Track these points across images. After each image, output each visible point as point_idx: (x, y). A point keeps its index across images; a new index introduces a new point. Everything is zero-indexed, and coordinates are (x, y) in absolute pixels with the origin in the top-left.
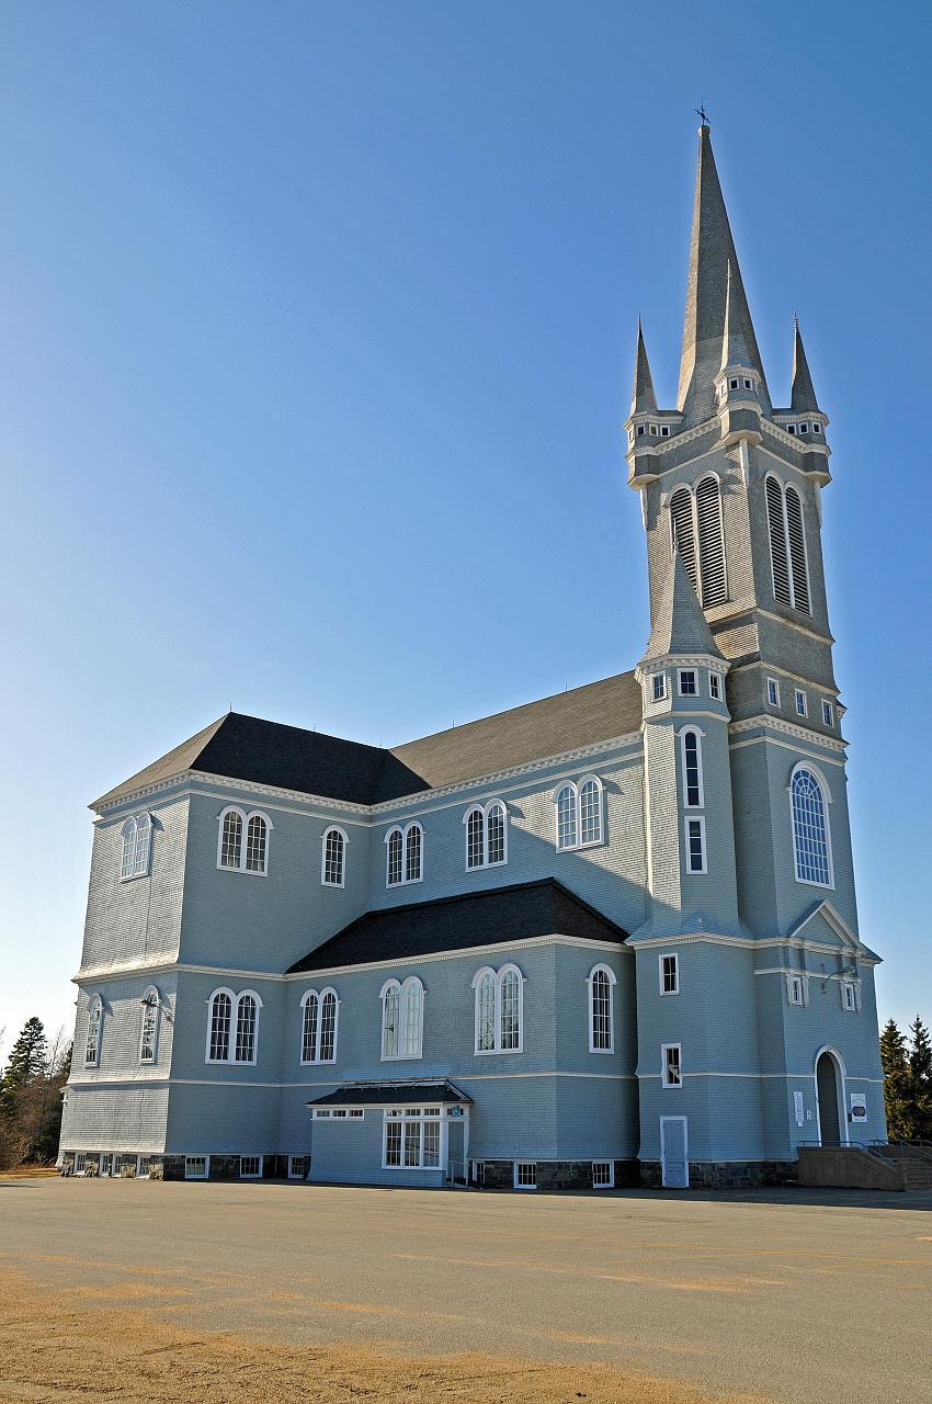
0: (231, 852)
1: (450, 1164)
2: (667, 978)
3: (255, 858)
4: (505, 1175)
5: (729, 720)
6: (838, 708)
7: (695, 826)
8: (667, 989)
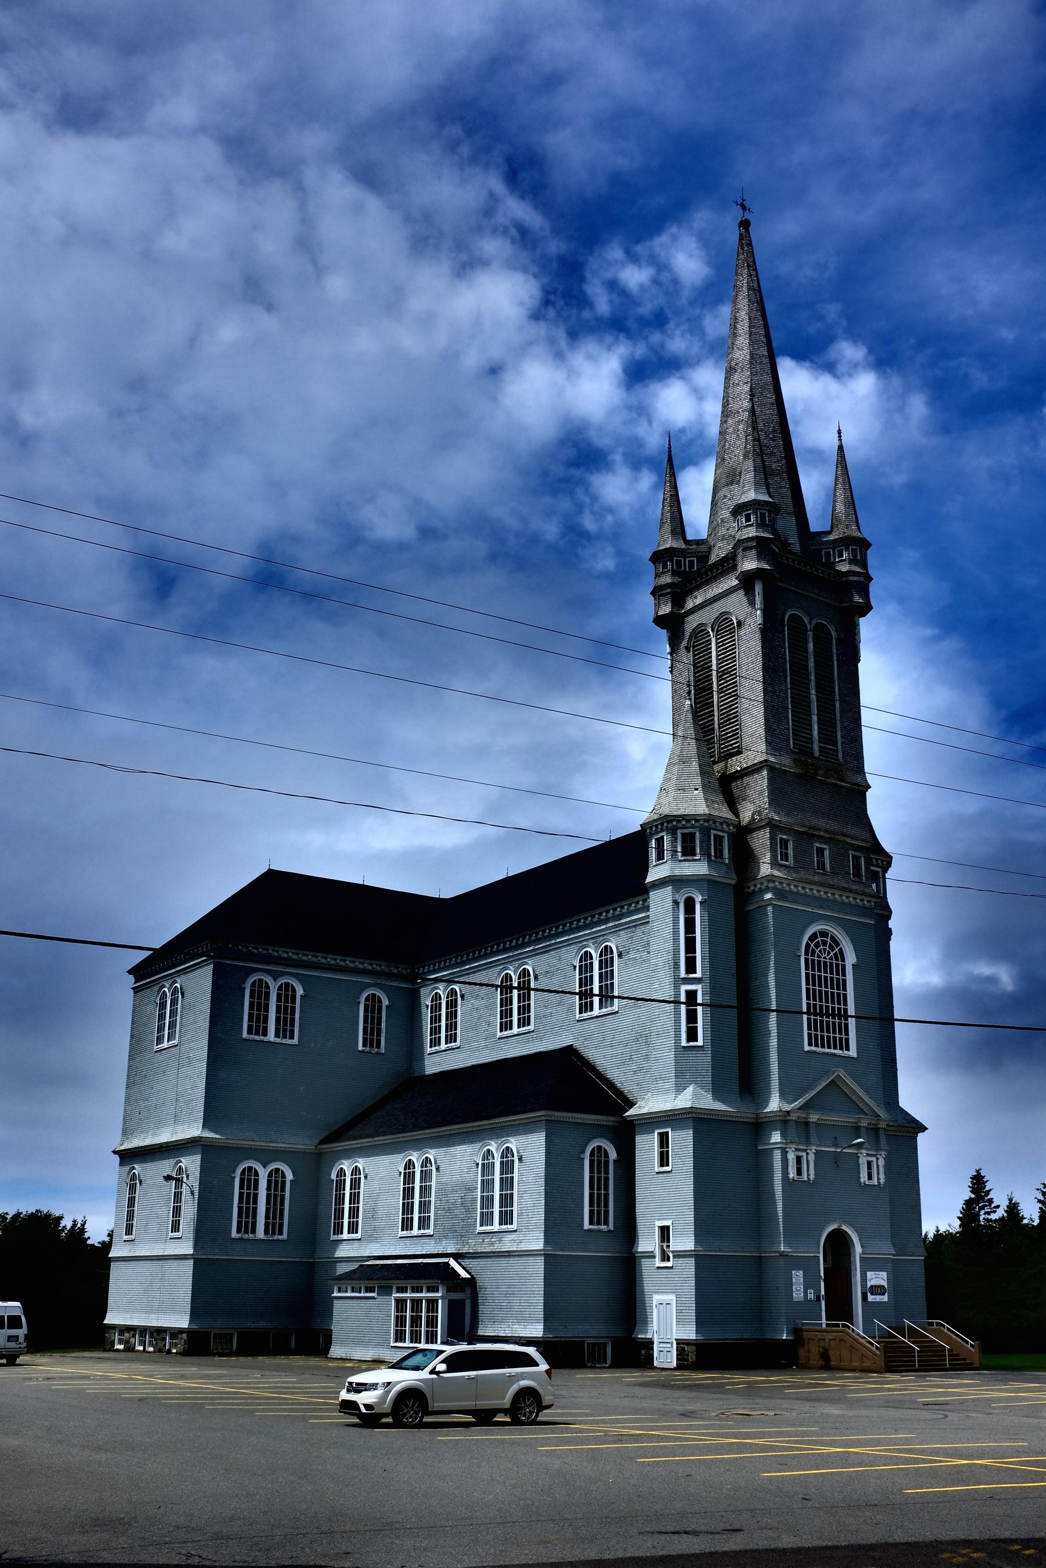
2: (662, 1154)
3: (284, 1027)
8: (662, 1165)
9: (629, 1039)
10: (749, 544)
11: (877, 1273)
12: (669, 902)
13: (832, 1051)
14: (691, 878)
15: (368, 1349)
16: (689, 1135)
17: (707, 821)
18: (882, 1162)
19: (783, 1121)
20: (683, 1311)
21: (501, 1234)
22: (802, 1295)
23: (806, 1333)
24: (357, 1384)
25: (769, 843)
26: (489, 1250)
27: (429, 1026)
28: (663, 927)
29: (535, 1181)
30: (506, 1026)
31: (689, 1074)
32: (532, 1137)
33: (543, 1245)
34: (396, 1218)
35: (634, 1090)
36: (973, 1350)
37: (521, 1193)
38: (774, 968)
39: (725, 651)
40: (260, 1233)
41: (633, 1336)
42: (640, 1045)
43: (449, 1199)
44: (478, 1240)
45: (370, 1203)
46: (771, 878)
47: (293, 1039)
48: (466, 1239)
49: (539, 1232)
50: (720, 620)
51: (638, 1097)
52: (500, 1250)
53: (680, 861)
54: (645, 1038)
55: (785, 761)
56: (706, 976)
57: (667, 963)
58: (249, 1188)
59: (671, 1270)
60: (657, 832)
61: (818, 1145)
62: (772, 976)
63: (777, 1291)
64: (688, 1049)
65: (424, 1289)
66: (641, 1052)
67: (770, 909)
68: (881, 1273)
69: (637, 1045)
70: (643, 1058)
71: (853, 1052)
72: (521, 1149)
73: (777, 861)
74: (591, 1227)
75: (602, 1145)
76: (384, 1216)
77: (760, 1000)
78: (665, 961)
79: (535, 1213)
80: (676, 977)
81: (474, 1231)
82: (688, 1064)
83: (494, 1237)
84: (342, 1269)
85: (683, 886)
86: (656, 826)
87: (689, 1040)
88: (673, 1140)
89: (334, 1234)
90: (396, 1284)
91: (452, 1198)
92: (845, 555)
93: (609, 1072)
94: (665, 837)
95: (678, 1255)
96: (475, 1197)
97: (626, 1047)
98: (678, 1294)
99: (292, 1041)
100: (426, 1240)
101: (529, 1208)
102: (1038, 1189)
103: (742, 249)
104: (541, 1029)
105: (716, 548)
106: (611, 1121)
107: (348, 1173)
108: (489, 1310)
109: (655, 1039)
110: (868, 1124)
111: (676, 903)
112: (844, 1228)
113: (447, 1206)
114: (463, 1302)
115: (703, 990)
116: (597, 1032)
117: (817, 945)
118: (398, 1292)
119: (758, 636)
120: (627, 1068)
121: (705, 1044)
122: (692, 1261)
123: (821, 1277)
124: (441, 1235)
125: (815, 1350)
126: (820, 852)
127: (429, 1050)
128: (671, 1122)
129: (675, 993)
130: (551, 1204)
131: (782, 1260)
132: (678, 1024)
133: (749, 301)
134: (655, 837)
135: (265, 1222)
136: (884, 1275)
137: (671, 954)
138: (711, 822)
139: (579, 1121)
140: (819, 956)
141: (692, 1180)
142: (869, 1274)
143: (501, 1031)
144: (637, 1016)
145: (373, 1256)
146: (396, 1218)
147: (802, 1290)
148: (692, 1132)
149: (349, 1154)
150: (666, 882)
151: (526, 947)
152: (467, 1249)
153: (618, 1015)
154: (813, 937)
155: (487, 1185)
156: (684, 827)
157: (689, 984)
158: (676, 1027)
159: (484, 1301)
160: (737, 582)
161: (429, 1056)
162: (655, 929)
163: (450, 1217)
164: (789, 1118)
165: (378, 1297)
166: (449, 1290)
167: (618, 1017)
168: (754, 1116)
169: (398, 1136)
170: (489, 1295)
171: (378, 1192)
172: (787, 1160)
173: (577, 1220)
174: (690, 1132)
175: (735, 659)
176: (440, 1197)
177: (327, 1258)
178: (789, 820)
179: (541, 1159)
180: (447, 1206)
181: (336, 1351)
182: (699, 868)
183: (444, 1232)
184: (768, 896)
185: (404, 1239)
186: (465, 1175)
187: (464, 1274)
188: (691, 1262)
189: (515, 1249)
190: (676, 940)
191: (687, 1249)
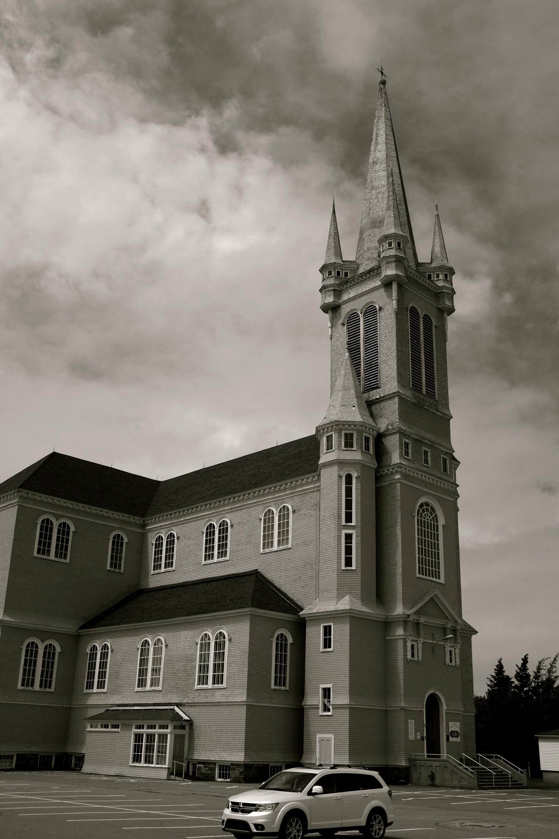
0: (44, 548)
1: (173, 763)
2: (325, 640)
3: (61, 551)
4: (210, 772)
5: (375, 467)
6: (453, 462)
7: (349, 537)
8: (325, 647)
10: (390, 260)
11: (455, 723)
12: (335, 476)
13: (431, 578)
14: (350, 461)
15: (111, 767)
16: (347, 628)
17: (361, 426)
18: (458, 651)
19: (405, 621)
20: (339, 745)
21: (214, 690)
22: (414, 736)
23: (418, 761)
24: (244, 804)
25: (398, 444)
26: (204, 701)
27: (153, 557)
28: (331, 492)
29: (241, 655)
30: (209, 557)
33: (246, 698)
34: (134, 679)
35: (302, 599)
36: (522, 775)
37: (229, 663)
38: (400, 522)
39: (369, 325)
40: (37, 687)
41: (301, 762)
42: (307, 569)
43: (175, 666)
44: (195, 695)
45: (115, 668)
46: (399, 465)
47: (66, 559)
48: (187, 693)
49: (243, 689)
50: (367, 307)
51: (305, 603)
52: (213, 701)
53: (343, 450)
54: (311, 565)
55: (408, 394)
56: (358, 525)
57: (333, 515)
58: (31, 656)
59: (331, 718)
60: (327, 432)
61: (425, 638)
62: (399, 527)
63: (398, 733)
64: (346, 572)
65: (157, 727)
66: (307, 574)
67: (398, 485)
68: (457, 723)
69: (305, 570)
70: (309, 578)
71: (442, 580)
72: (231, 633)
73: (403, 455)
74: (276, 687)
75: (284, 633)
76: (125, 677)
77: (389, 543)
78: (331, 514)
80: (339, 524)
81: (193, 688)
83: (208, 692)
84: (92, 712)
85: (344, 467)
86: (328, 428)
87: (346, 566)
88: (334, 630)
89: (87, 689)
90: (158, 723)
91: (176, 666)
92: (441, 277)
93: (283, 587)
94: (333, 435)
95: (336, 707)
96: (194, 665)
97: (297, 571)
98: (335, 733)
99: (66, 560)
100: (156, 694)
101: (236, 673)
102: (488, 678)
103: (381, 96)
104: (235, 559)
105: (364, 265)
106: (290, 618)
107: (99, 649)
108: (202, 742)
111: (340, 477)
112: (437, 693)
113: (172, 671)
114: (183, 736)
117: (423, 511)
118: (136, 728)
119: (393, 316)
120: (297, 585)
121: (357, 568)
122: (347, 711)
123: (424, 724)
124: (167, 690)
125: (425, 774)
126: (426, 453)
127: (152, 572)
130: (251, 671)
131: (403, 712)
132: (339, 555)
133: (386, 125)
134: (326, 435)
135: (41, 679)
136: (458, 724)
137: (335, 509)
138: (364, 428)
139: (271, 616)
140: (424, 518)
141: (349, 657)
142: (450, 723)
143: (205, 560)
144: (305, 551)
145: (115, 704)
146: (134, 679)
147: (414, 733)
148: (349, 626)
149: (99, 636)
150: (333, 464)
151: (226, 507)
152: (187, 700)
153: (291, 550)
154: (421, 506)
155: (204, 658)
157: (347, 529)
158: (338, 557)
159: (199, 736)
160: (380, 283)
161: (153, 576)
162: (324, 494)
163: (175, 678)
164: (409, 619)
165: (121, 732)
166: (175, 727)
169: (138, 624)
170: (202, 732)
171: (121, 661)
172: (406, 647)
173: (267, 682)
174: (347, 626)
175: (377, 330)
176: (168, 665)
177: (80, 705)
178: (410, 430)
180: (172, 671)
181: (87, 768)
182: (355, 455)
183: (170, 689)
184: (398, 476)
185: (139, 693)
186: (187, 651)
187: (186, 717)
188: (346, 712)
189: (224, 701)
190: (339, 501)
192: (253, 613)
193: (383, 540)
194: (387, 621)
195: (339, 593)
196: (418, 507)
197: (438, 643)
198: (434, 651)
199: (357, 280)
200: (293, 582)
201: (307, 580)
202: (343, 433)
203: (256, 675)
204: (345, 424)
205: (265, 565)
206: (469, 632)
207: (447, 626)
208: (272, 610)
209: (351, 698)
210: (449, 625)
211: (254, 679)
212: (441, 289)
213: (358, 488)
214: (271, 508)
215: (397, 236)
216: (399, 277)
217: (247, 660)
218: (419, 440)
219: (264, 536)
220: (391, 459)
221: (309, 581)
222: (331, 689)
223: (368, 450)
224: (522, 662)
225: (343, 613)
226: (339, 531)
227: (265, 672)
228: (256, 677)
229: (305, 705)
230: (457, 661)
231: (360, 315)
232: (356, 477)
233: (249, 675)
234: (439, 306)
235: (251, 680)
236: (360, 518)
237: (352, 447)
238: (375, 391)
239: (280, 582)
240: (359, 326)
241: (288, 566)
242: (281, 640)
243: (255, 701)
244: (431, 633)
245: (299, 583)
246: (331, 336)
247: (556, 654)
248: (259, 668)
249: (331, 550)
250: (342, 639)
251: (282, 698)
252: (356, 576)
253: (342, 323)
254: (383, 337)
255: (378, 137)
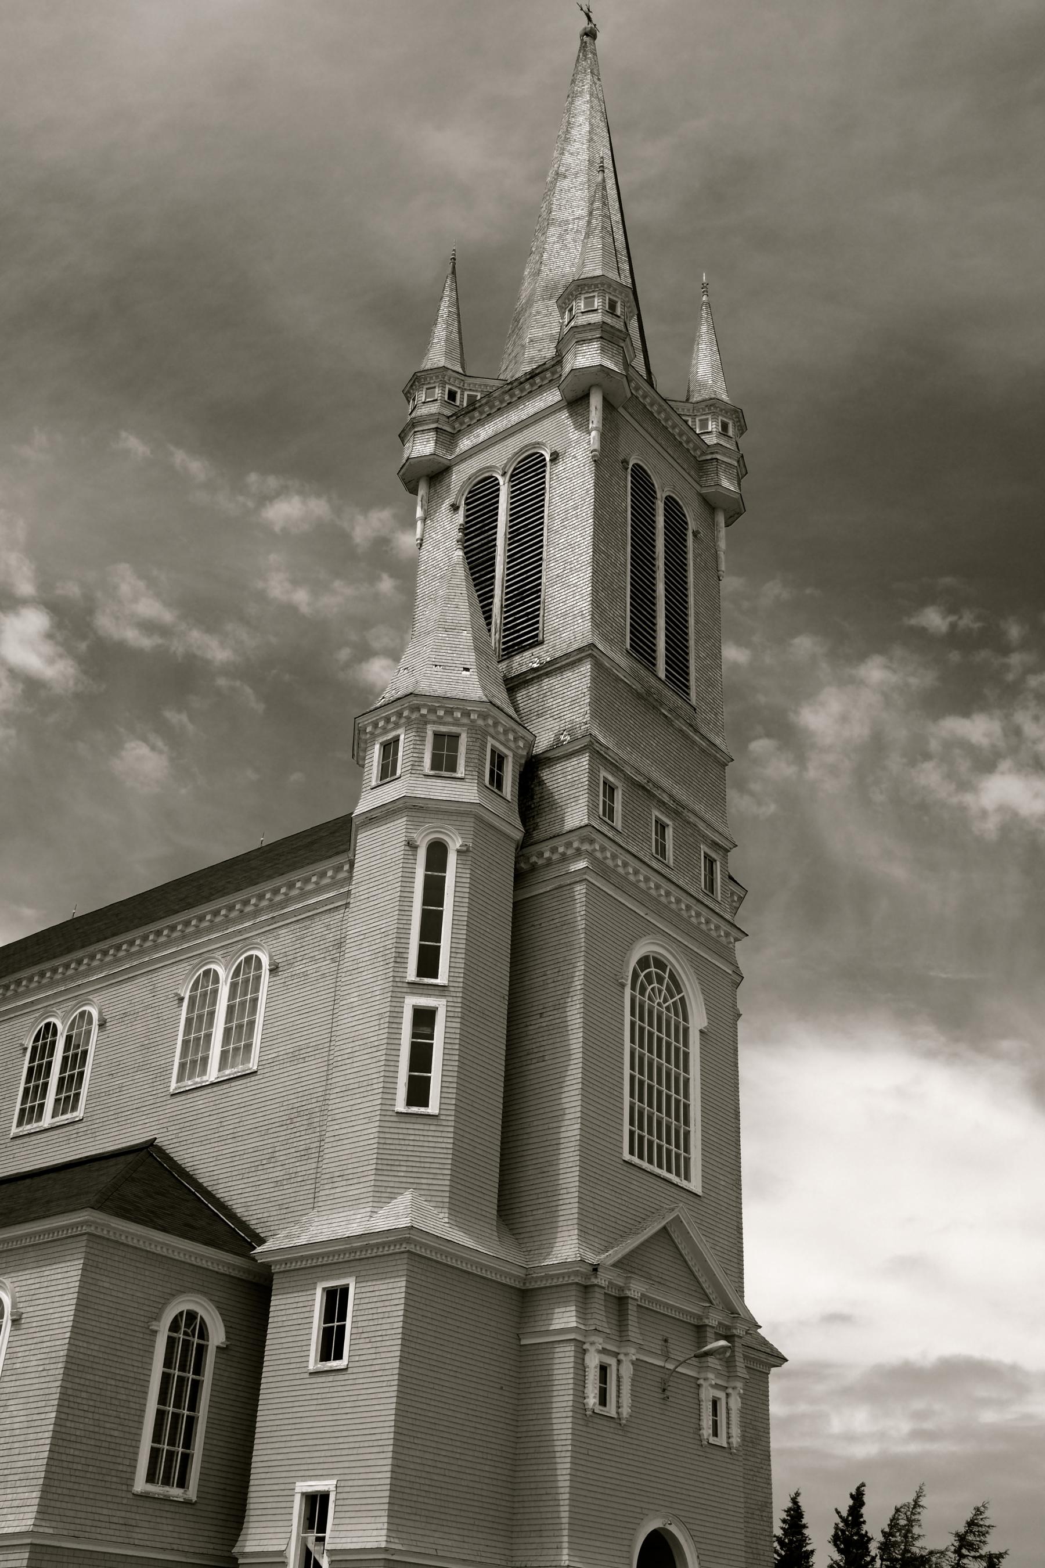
2: (327, 1333)
7: (424, 1018)
8: (325, 1357)
9: (273, 1121)
14: (444, 806)
16: (397, 1290)
17: (484, 716)
18: (735, 1403)
29: (41, 1368)
30: (30, 1113)
31: (404, 1169)
32: (53, 1272)
55: (620, 659)
56: (456, 985)
60: (385, 731)
64: (407, 1119)
67: (580, 890)
70: (298, 1154)
71: (695, 1184)
72: (23, 1299)
74: (152, 1488)
79: (29, 1443)
80: (397, 979)
82: (404, 1148)
86: (387, 720)
87: (410, 1102)
88: (357, 1302)
92: (711, 426)
94: (402, 737)
101: (17, 1432)
109: (338, 1100)
110: (720, 1323)
111: (411, 846)
112: (673, 1529)
115: (449, 1009)
116: (208, 1114)
120: (262, 1177)
121: (443, 1112)
126: (662, 827)
128: (357, 1263)
129: (393, 1009)
130: (68, 1424)
132: (392, 1069)
138: (490, 722)
148: (404, 1284)
153: (257, 1078)
154: (644, 963)
156: (440, 721)
157: (421, 995)
162: (362, 897)
164: (595, 1281)
167: (256, 1083)
168: (521, 1273)
173: (120, 1468)
179: (65, 1319)
184: (582, 864)
190: (404, 912)
191: (369, 1546)
192: (99, 1233)
193: (527, 1047)
194: (529, 1286)
195: (379, 1183)
196: (633, 963)
197: (679, 1369)
198: (667, 1393)
199: (497, 403)
200: (253, 1169)
201: (294, 1160)
202: (430, 730)
203: (84, 1440)
204: (437, 705)
205: (177, 1127)
206: (764, 1356)
207: (706, 1321)
208: (164, 1230)
209: (393, 1529)
210: (714, 1319)
211: (77, 1453)
212: (712, 453)
213: (464, 880)
214: (213, 966)
215: (610, 286)
216: (608, 374)
217: (59, 1383)
218: (644, 788)
219: (186, 1043)
220: (563, 820)
221: (298, 1164)
222: (332, 1498)
223: (500, 786)
224: (851, 1502)
225: (388, 1244)
226: (397, 1000)
227: (116, 1433)
228: (84, 1447)
229: (245, 1555)
230: (733, 1434)
231: (501, 480)
232: (458, 851)
233: (60, 1439)
234: (704, 491)
235: (64, 1457)
236: (463, 966)
237: (454, 770)
238: (527, 654)
239: (215, 1173)
240: (493, 537)
241: (241, 1124)
242: (185, 1333)
243: (65, 1532)
244: (660, 1338)
245: (269, 1171)
246: (422, 540)
247: (918, 1489)
248: (97, 1417)
249: (367, 1057)
250: (378, 1327)
251: (171, 1528)
252: (439, 1134)
253: (452, 506)
254: (557, 522)
255: (571, 128)
